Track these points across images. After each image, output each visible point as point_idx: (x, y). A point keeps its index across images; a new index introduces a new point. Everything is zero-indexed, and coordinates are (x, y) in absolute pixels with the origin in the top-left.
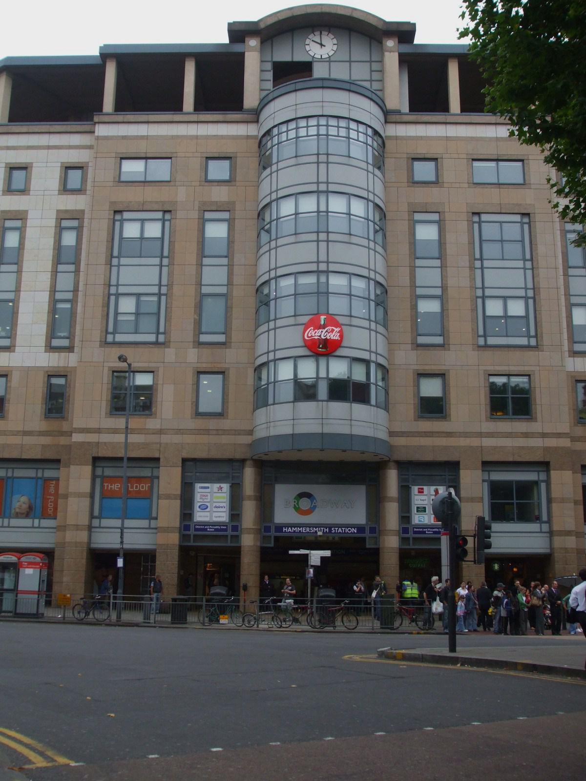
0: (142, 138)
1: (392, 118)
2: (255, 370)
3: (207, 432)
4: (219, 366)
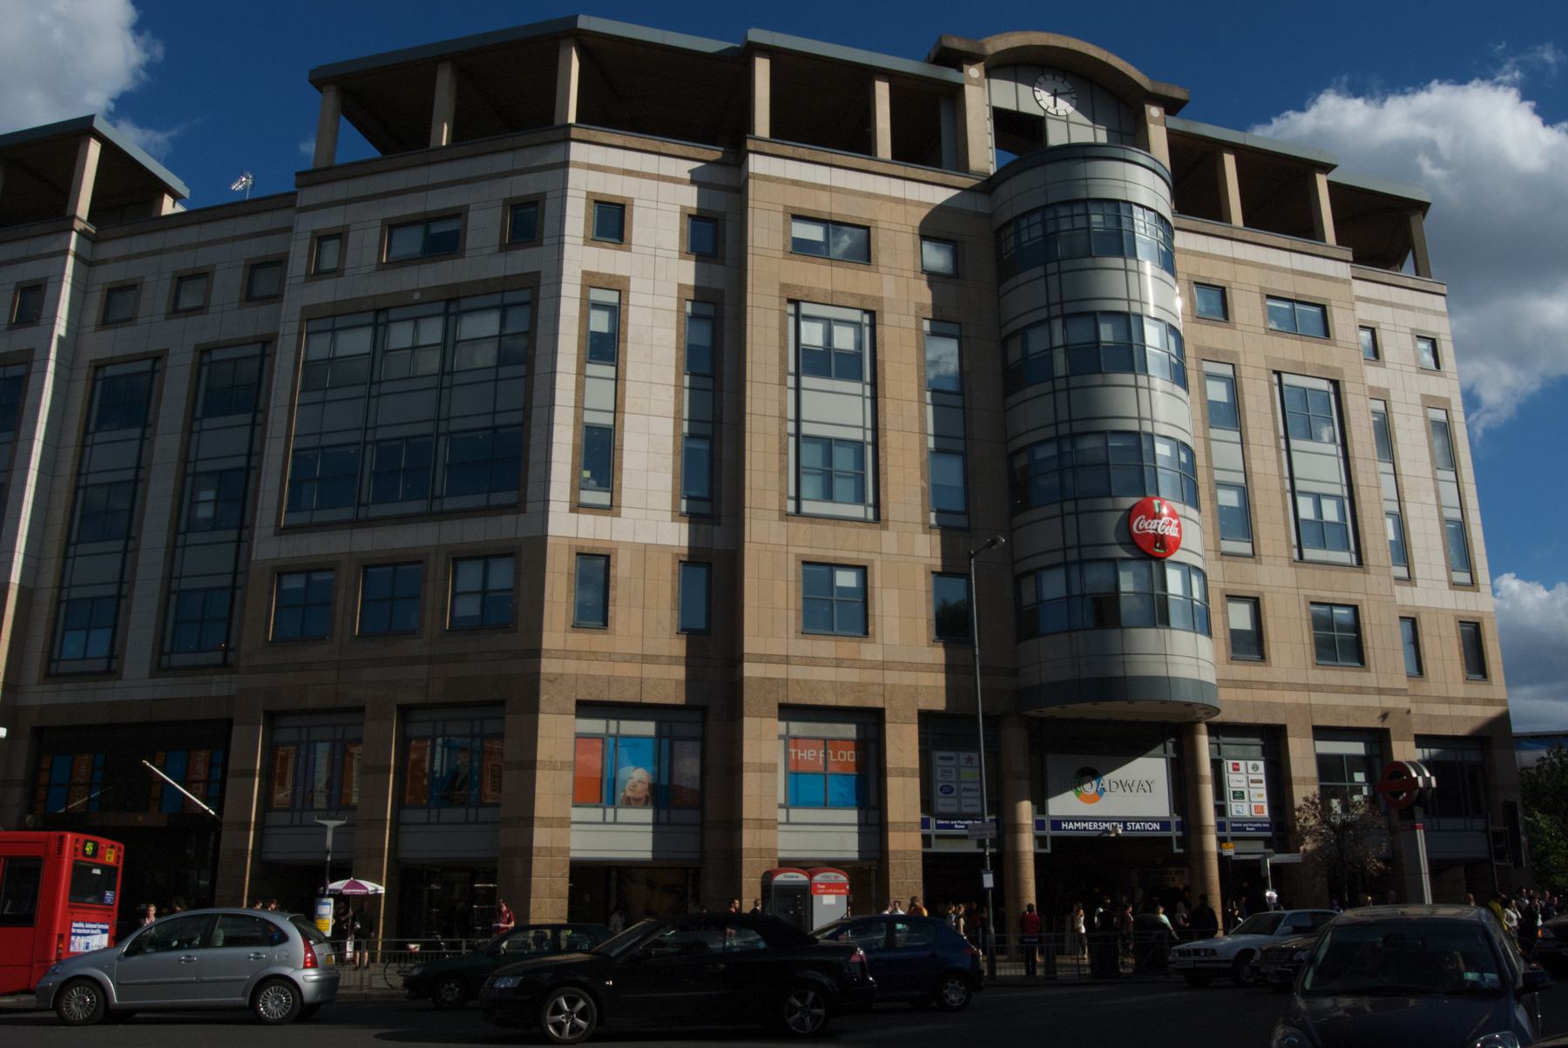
0: (823, 187)
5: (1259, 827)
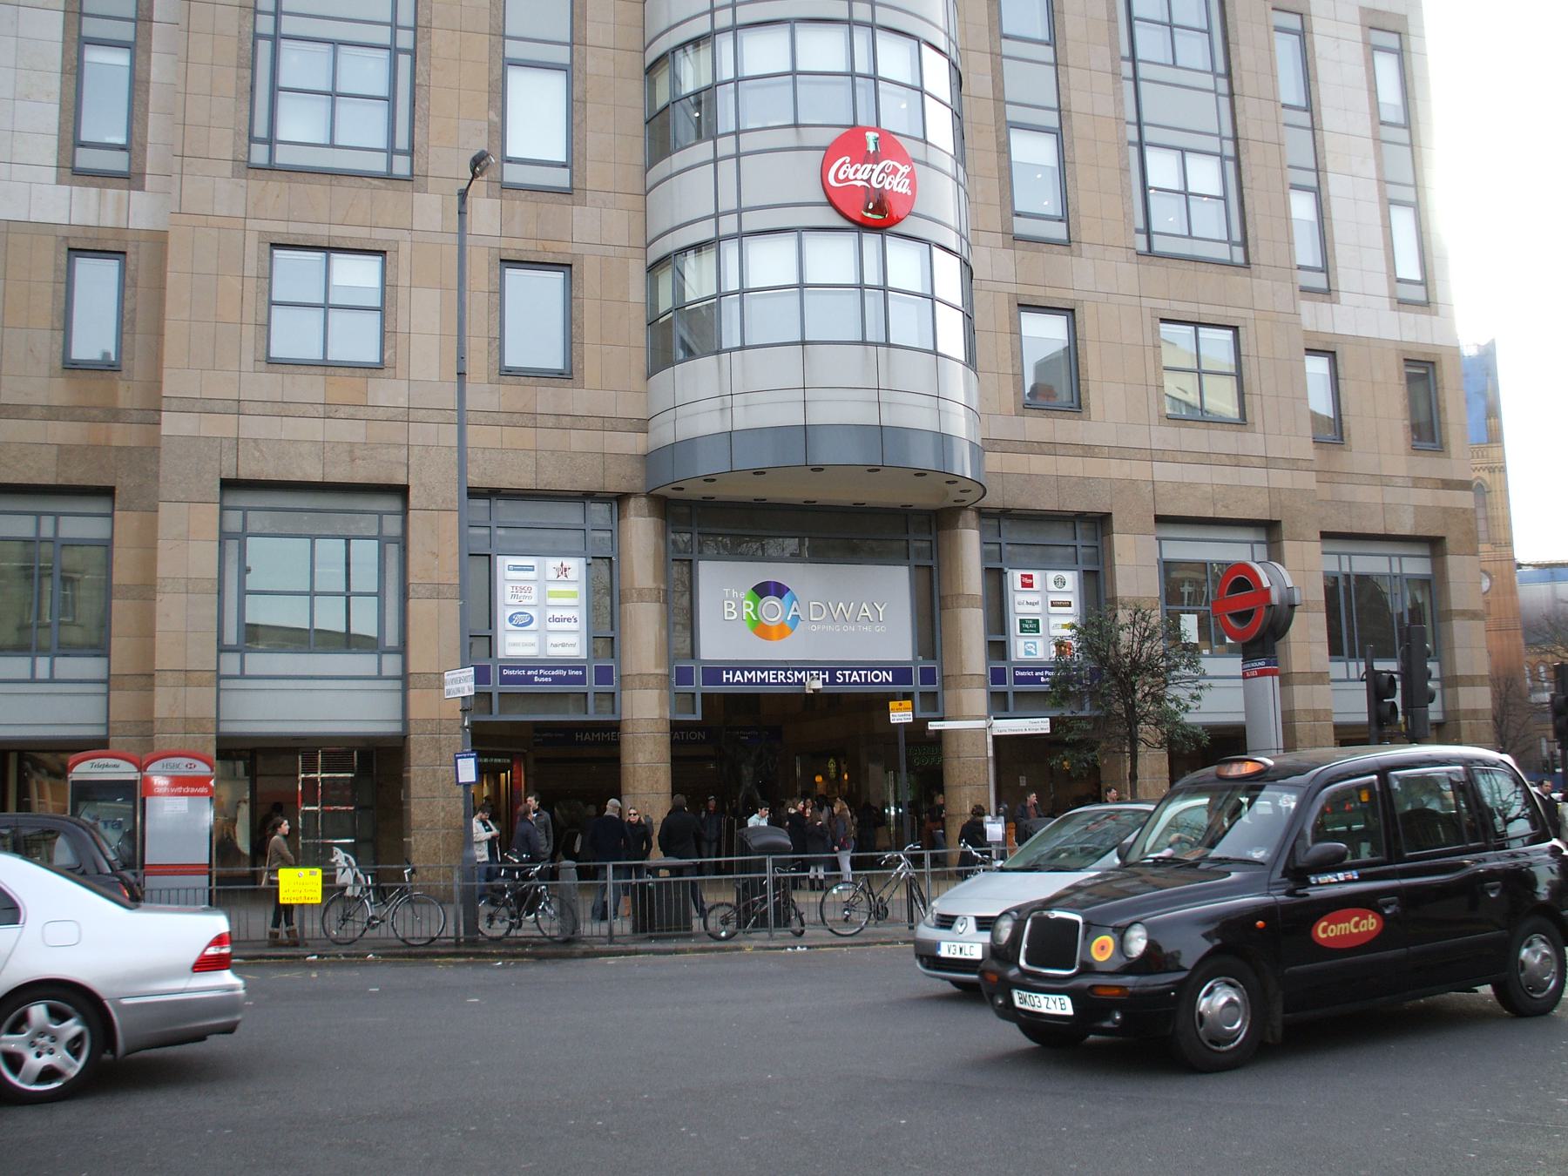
3: (529, 419)
4: (561, 247)
5: (560, 676)
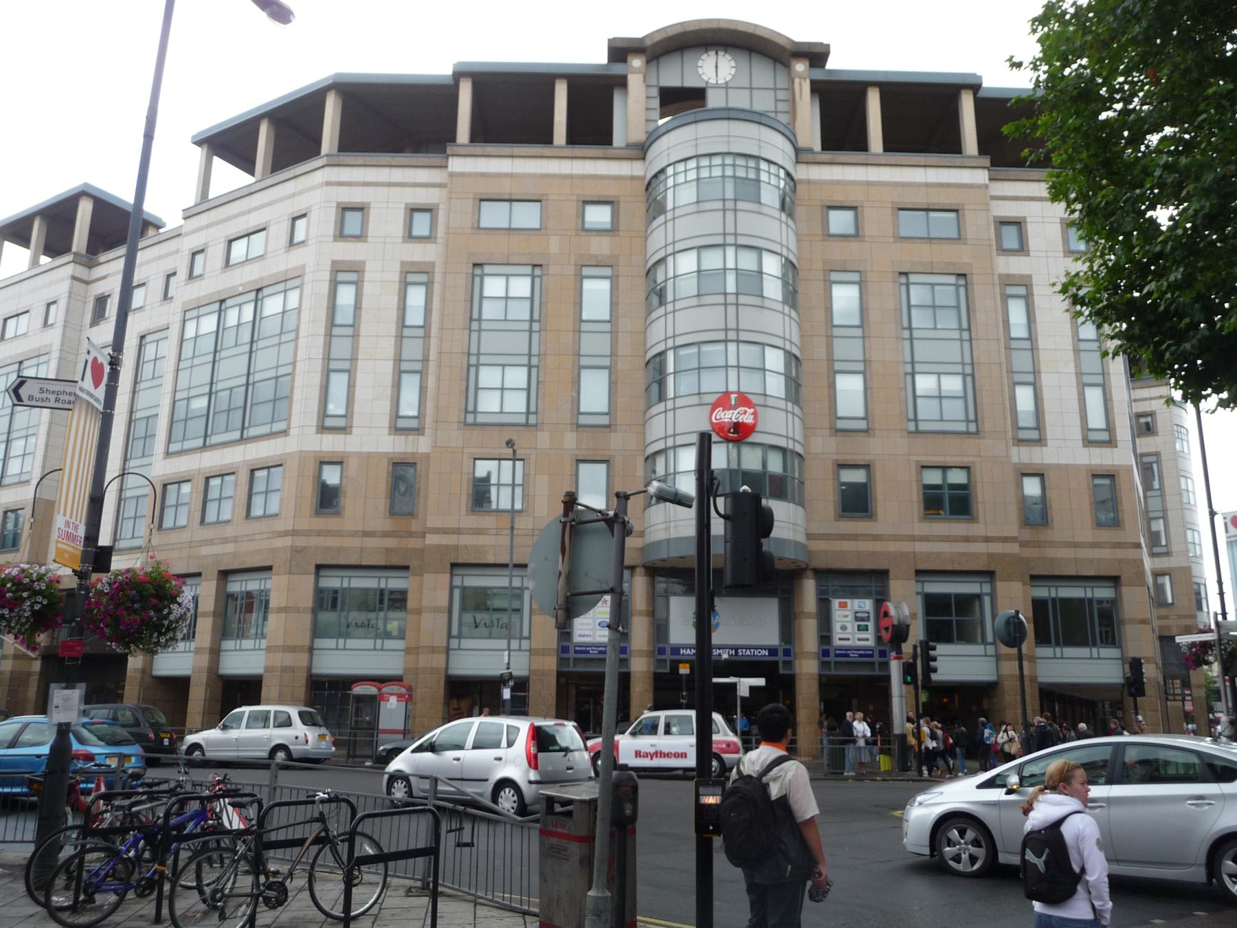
0: (506, 175)
1: (804, 157)
2: (646, 459)
